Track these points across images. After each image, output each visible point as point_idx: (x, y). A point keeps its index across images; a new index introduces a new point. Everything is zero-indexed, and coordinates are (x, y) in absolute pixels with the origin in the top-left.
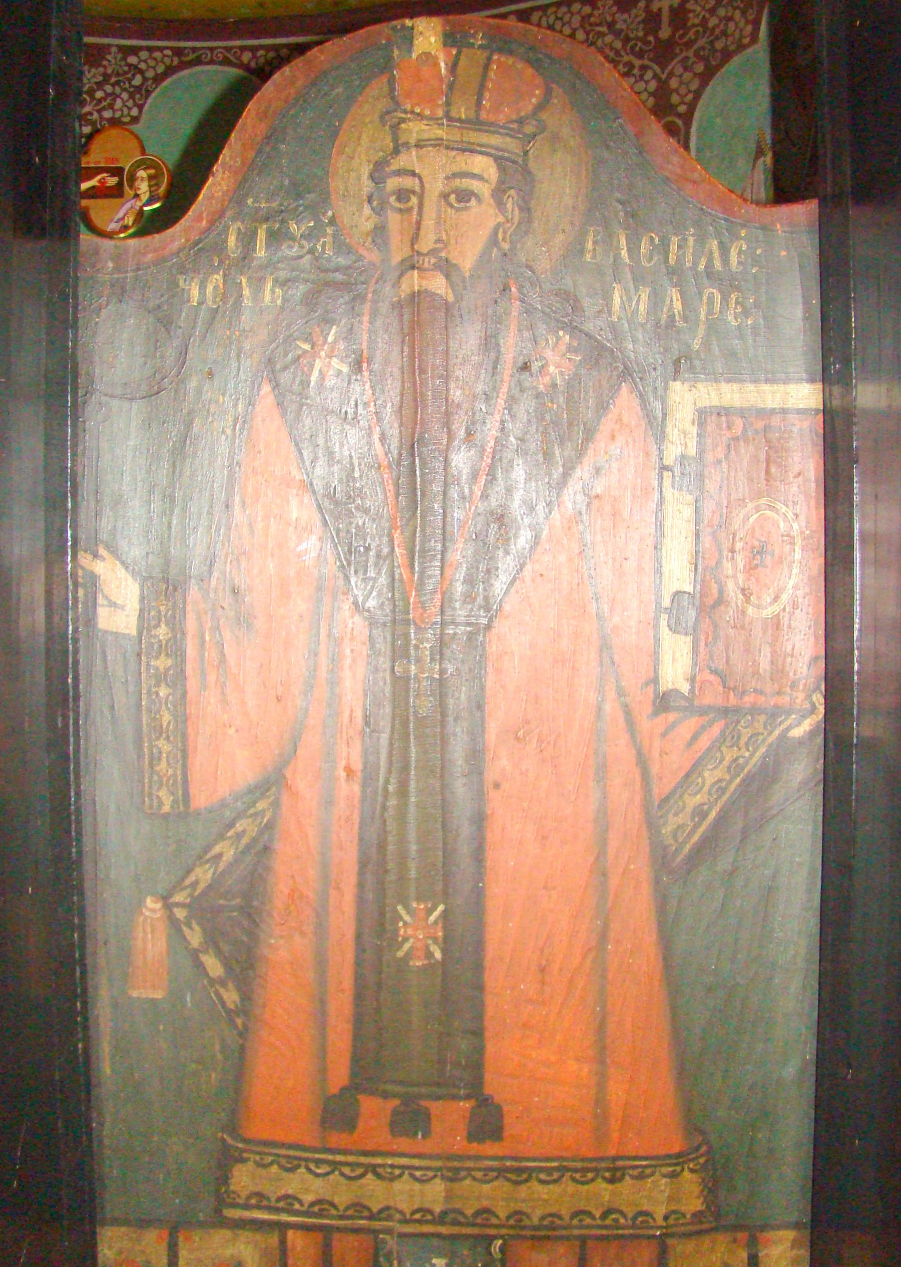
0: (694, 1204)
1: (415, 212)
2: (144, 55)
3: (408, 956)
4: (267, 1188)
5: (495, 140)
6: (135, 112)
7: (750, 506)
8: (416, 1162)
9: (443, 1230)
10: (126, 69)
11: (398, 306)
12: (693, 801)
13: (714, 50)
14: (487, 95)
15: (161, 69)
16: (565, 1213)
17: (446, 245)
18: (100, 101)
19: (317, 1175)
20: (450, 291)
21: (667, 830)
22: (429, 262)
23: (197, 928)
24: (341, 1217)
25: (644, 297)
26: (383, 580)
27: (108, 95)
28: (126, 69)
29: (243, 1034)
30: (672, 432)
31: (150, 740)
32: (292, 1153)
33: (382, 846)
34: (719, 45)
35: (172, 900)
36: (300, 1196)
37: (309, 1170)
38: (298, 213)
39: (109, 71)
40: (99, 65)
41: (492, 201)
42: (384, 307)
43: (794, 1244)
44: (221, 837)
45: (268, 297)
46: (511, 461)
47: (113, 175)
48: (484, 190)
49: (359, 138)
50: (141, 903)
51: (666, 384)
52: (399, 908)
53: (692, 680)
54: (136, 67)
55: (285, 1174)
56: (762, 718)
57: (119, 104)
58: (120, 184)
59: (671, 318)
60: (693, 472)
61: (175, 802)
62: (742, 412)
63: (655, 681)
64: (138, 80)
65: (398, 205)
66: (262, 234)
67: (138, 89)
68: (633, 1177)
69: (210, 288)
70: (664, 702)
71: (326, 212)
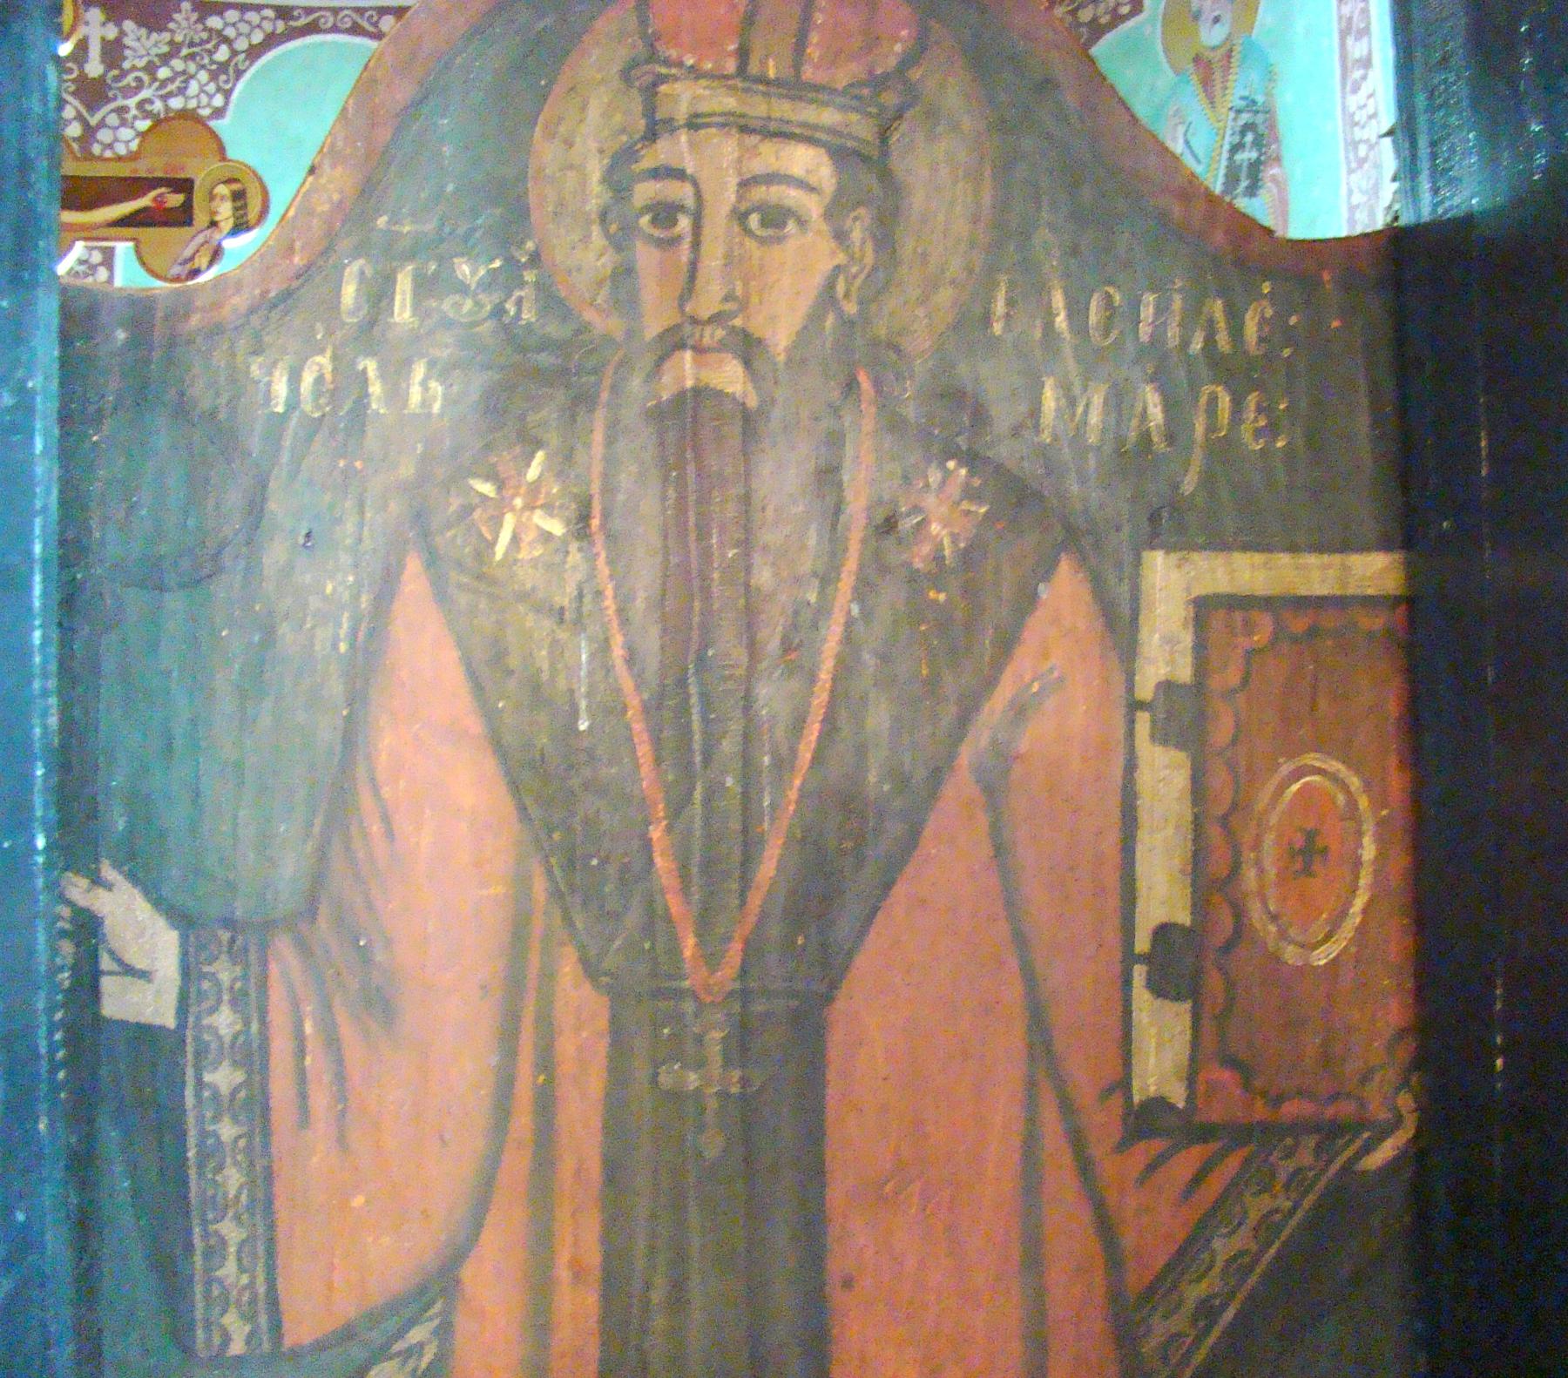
1: (686, 245)
5: (829, 117)
6: (218, 101)
10: (205, 35)
11: (659, 415)
12: (1194, 1292)
14: (814, 38)
15: (257, 38)
17: (744, 305)
18: (164, 83)
20: (750, 387)
21: (1150, 1346)
22: (712, 336)
26: (633, 918)
27: (177, 74)
28: (205, 35)
31: (205, 1223)
38: (470, 244)
39: (179, 38)
40: (166, 29)
41: (824, 227)
42: (630, 415)
45: (415, 395)
46: (864, 700)
47: (177, 191)
48: (813, 206)
49: (583, 108)
53: (1191, 1082)
54: (219, 33)
56: (1310, 1142)
57: (193, 87)
58: (187, 207)
59: (1146, 437)
60: (1183, 715)
62: (1267, 603)
64: (223, 54)
65: (657, 233)
66: (404, 283)
67: (223, 67)
70: (1146, 1120)
71: (523, 242)
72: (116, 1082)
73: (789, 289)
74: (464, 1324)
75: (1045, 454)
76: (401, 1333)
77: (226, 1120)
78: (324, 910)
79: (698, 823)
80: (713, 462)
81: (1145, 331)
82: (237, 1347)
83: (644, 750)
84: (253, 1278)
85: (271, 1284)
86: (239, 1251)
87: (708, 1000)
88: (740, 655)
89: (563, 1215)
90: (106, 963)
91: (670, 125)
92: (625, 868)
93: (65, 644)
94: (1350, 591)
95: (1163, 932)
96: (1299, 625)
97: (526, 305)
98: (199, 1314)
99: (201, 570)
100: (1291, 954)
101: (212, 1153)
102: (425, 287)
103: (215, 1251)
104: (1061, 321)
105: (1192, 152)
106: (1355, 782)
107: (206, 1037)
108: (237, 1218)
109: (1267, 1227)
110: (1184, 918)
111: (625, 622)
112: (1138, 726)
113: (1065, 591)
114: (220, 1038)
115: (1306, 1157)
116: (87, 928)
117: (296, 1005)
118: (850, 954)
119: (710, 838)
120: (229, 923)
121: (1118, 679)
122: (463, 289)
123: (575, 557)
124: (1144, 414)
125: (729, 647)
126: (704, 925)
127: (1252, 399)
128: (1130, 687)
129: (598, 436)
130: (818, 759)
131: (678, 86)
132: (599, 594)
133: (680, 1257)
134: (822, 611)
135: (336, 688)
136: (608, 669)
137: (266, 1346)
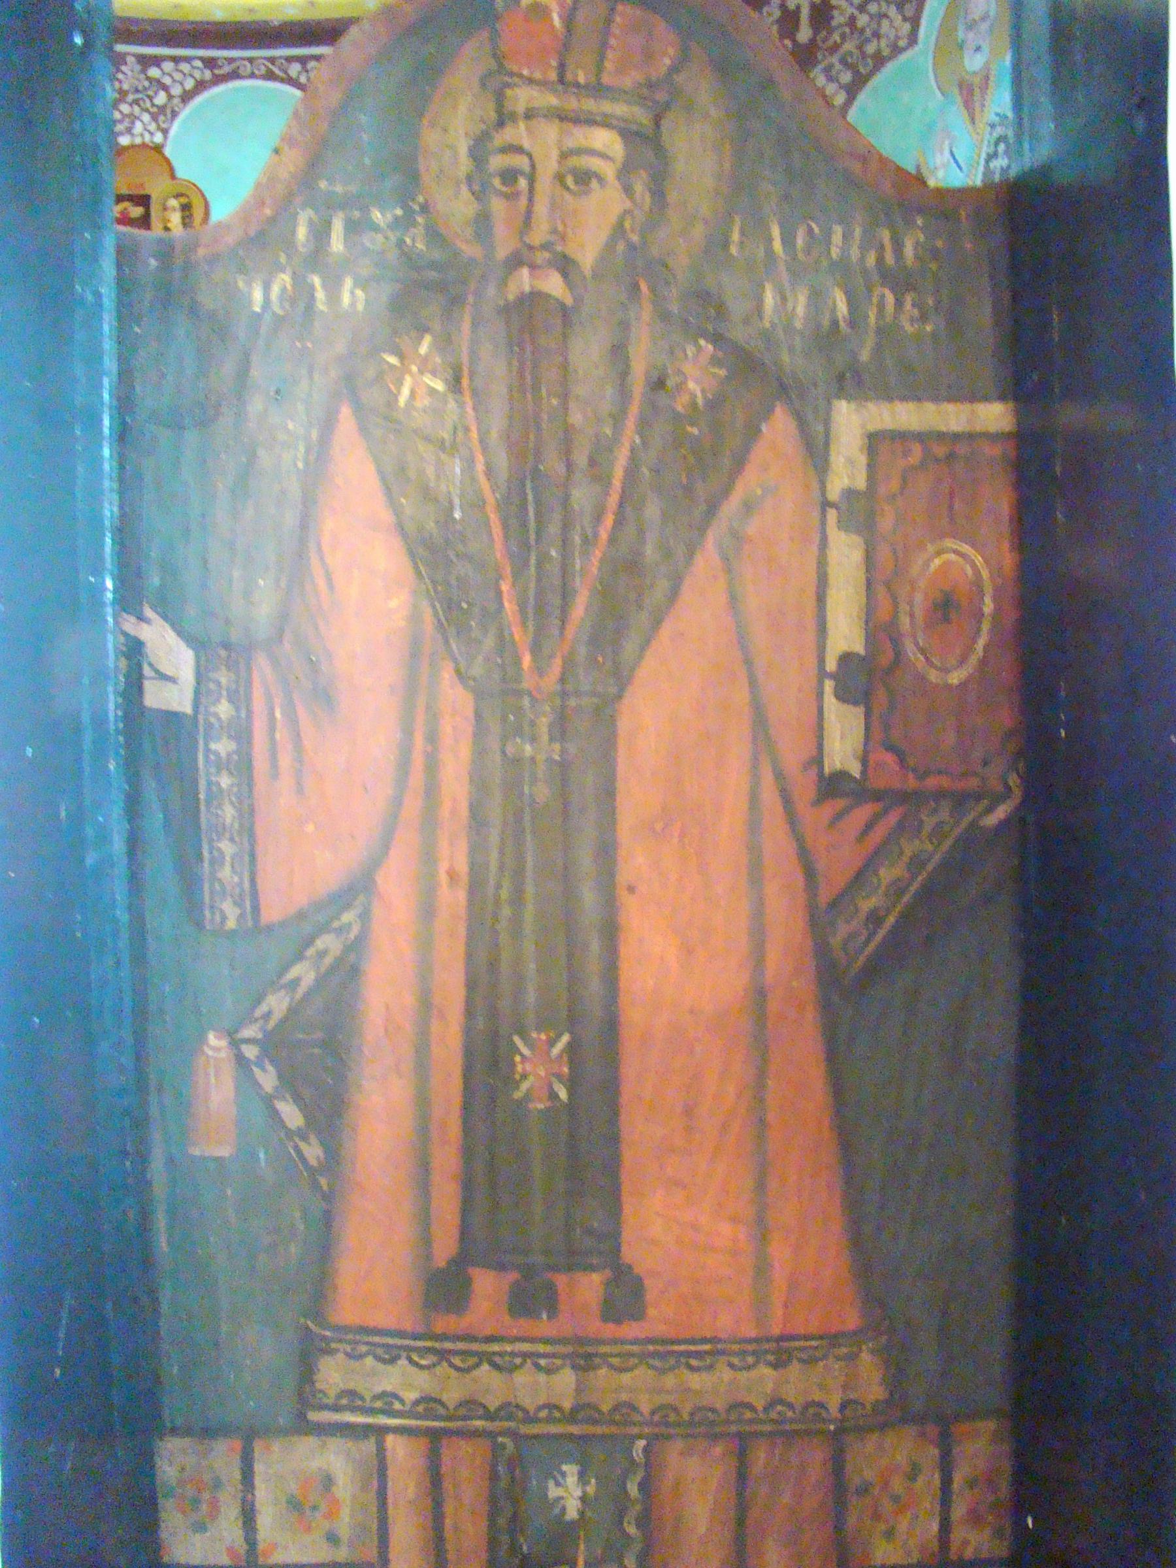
0: (873, 1389)
2: (168, 66)
3: (528, 1097)
4: (361, 1386)
5: (620, 109)
7: (931, 548)
8: (541, 1348)
9: (575, 1430)
12: (867, 904)
13: (864, 55)
14: (610, 55)
15: (190, 84)
16: (720, 1405)
17: (563, 238)
19: (421, 1367)
23: (271, 1068)
24: (450, 1418)
25: (802, 299)
26: (490, 642)
28: (147, 84)
29: (328, 1197)
30: (838, 460)
31: (211, 841)
32: (390, 1341)
33: (493, 965)
34: (871, 49)
35: (240, 1036)
36: (401, 1393)
37: (410, 1360)
39: (126, 87)
43: (995, 1438)
44: (299, 957)
45: (346, 299)
47: (138, 204)
48: (609, 171)
50: (202, 1039)
51: (829, 403)
52: (517, 1039)
53: (864, 761)
54: (158, 81)
55: (380, 1366)
59: (835, 323)
60: (860, 511)
61: (242, 916)
62: (921, 437)
63: (818, 759)
64: (161, 99)
65: (504, 189)
67: (162, 109)
68: (801, 1360)
69: (276, 290)
70: (832, 786)
72: (153, 745)
73: (594, 223)
74: (377, 911)
75: (768, 337)
76: (337, 917)
77: (224, 772)
78: (288, 637)
79: (533, 585)
80: (542, 341)
81: (835, 253)
82: (231, 924)
83: (497, 530)
84: (241, 879)
85: (253, 881)
86: (232, 859)
87: (538, 696)
88: (561, 469)
89: (443, 844)
90: (147, 670)
91: (513, 117)
92: (484, 609)
93: (122, 467)
94: (978, 429)
95: (846, 659)
96: (940, 451)
97: (419, 239)
98: (207, 900)
99: (205, 414)
100: (933, 676)
101: (215, 794)
102: (353, 228)
103: (217, 861)
104: (777, 246)
105: (956, 162)
106: (979, 560)
107: (212, 720)
108: (232, 840)
109: (917, 863)
110: (859, 648)
111: (485, 449)
112: (829, 517)
113: (780, 427)
114: (219, 719)
115: (944, 814)
116: (134, 650)
117: (269, 696)
118: (632, 669)
119: (540, 593)
120: (226, 646)
121: (815, 485)
122: (376, 228)
123: (452, 405)
124: (834, 310)
125: (553, 464)
126: (536, 649)
127: (909, 300)
128: (823, 494)
129: (466, 326)
130: (612, 540)
131: (517, 90)
132: (467, 429)
133: (519, 873)
134: (616, 439)
135: (295, 490)
136: (473, 479)
137: (250, 924)
